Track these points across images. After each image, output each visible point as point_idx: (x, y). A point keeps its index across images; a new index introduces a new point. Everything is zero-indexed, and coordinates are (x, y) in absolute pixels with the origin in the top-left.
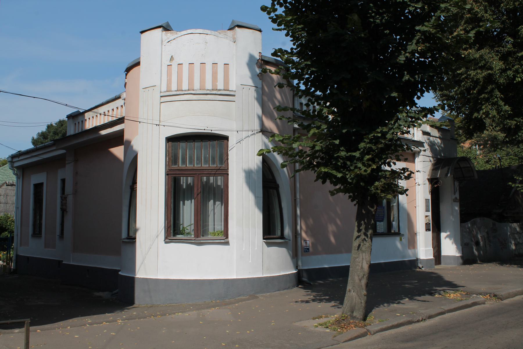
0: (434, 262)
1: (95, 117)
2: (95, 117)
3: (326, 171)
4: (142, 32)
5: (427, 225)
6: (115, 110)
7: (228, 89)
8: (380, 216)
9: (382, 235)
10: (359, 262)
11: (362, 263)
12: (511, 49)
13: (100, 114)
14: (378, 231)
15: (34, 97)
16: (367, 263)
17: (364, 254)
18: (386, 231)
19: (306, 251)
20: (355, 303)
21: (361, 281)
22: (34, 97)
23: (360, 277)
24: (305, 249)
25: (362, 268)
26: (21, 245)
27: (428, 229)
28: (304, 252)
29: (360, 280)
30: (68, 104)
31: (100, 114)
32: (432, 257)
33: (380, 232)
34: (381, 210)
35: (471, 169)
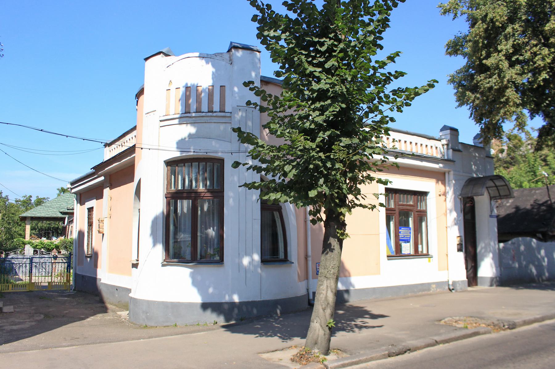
1: (116, 148)
2: (116, 148)
3: (316, 193)
4: (146, 59)
5: (460, 245)
6: (131, 139)
7: (224, 111)
8: (405, 237)
9: (408, 256)
10: (324, 290)
11: (327, 292)
12: (502, 4)
13: (119, 145)
14: (403, 252)
15: (7, 124)
16: (332, 292)
17: (329, 281)
18: (412, 252)
20: (318, 335)
21: (325, 311)
22: (7, 124)
23: (324, 306)
25: (326, 297)
26: (78, 265)
27: (460, 250)
29: (324, 310)
30: (44, 129)
31: (119, 145)
34: (407, 231)
35: (193, 135)
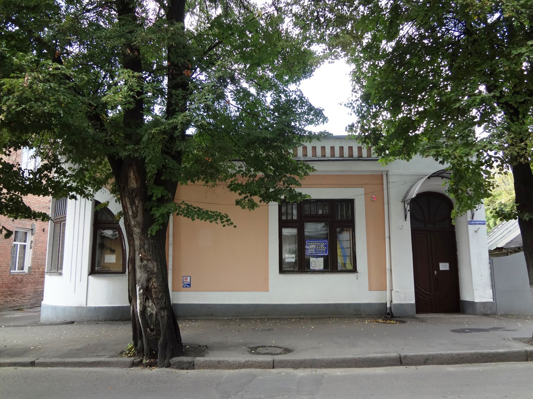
0: (414, 309)
19: (186, 287)
24: (185, 284)
28: (183, 287)
32: (413, 302)
33: (317, 269)
